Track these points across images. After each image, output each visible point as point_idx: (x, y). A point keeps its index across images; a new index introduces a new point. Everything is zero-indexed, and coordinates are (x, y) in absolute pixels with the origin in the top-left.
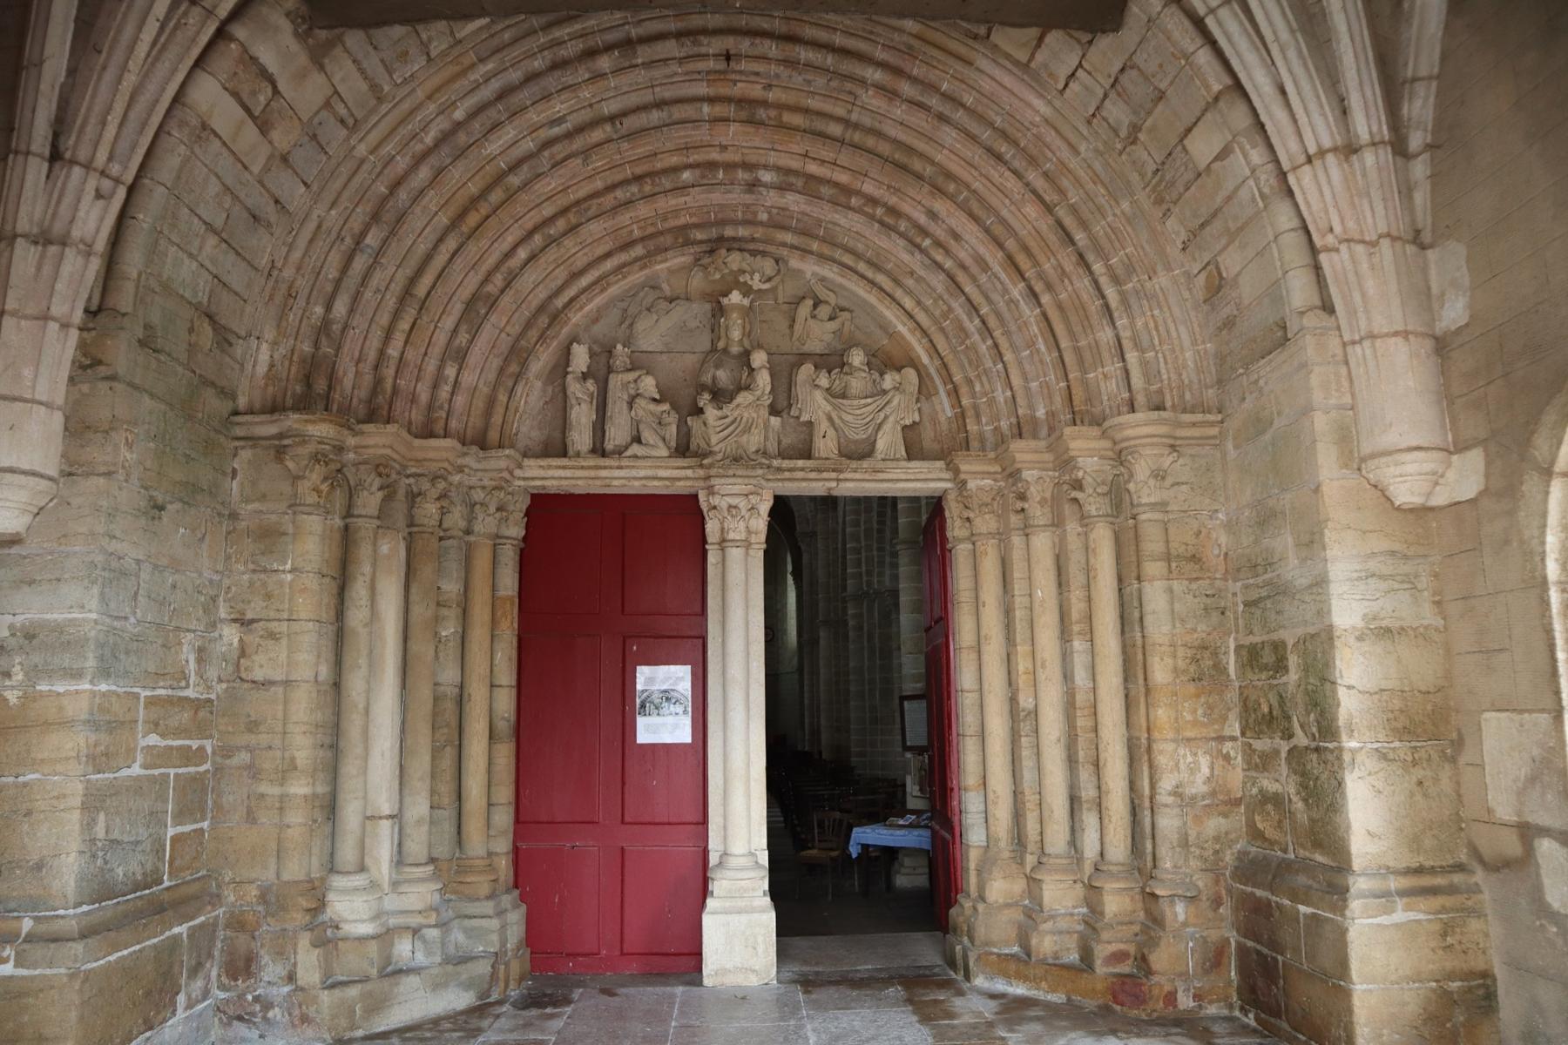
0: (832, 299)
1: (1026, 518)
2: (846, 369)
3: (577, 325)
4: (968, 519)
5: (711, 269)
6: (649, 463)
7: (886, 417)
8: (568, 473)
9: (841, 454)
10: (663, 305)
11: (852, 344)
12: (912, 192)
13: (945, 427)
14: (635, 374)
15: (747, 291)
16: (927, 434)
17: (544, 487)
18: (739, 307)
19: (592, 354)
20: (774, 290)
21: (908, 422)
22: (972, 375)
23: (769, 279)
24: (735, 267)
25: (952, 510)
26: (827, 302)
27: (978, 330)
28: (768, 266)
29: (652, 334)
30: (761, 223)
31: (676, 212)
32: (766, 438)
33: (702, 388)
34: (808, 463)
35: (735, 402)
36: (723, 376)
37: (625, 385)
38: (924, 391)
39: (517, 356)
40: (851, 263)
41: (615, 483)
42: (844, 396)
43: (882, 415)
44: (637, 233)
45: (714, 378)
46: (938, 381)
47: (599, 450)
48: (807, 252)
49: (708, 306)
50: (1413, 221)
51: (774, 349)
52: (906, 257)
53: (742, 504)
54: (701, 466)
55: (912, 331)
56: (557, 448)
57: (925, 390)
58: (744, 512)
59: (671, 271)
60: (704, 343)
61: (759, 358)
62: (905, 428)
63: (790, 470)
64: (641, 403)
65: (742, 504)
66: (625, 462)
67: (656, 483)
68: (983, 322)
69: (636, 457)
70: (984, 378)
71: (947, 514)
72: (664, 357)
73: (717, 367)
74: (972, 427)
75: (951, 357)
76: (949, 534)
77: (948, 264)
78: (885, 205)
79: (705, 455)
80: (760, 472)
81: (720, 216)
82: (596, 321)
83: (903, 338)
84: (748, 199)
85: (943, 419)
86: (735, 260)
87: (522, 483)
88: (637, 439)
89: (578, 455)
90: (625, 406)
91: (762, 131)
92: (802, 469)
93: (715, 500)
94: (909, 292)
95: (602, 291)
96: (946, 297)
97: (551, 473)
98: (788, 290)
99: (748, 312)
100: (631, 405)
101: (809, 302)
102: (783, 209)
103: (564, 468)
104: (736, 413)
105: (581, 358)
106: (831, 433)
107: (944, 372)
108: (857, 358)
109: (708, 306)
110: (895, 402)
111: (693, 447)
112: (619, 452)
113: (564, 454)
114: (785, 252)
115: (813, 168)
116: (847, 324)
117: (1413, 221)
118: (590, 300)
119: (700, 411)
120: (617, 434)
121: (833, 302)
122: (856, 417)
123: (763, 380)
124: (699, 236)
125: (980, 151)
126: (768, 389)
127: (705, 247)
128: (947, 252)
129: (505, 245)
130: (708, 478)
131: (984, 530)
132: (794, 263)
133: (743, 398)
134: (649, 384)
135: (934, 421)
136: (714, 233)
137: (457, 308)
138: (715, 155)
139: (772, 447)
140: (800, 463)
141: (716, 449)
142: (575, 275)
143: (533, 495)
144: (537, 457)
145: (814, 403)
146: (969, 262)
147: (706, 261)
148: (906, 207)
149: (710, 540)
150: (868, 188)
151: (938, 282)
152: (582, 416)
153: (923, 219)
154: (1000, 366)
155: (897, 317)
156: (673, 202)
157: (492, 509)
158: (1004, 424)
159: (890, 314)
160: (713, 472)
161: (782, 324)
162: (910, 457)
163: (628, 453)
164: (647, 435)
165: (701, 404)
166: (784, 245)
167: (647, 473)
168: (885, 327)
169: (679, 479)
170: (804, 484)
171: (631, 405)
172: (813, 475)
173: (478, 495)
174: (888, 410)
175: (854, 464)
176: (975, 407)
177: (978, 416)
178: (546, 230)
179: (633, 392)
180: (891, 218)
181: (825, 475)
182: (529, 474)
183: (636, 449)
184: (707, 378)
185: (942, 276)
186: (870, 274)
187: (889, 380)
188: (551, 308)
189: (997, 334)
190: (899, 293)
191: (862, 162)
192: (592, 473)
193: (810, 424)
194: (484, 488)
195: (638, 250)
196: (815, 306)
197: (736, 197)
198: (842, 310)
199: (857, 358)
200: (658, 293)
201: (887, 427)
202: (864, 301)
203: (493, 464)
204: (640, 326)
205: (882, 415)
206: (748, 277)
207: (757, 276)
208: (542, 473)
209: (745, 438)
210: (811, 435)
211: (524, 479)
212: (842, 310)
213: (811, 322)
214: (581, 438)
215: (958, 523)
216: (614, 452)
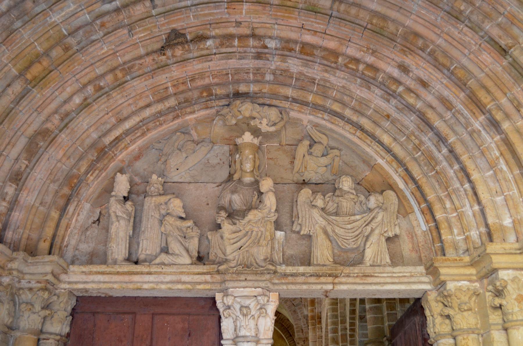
0: (324, 140)
1: (504, 314)
2: (338, 193)
3: (123, 161)
4: (448, 317)
5: (228, 117)
6: (173, 269)
7: (372, 230)
8: (106, 278)
9: (335, 262)
10: (191, 146)
11: (340, 174)
12: (386, 53)
13: (421, 239)
14: (168, 197)
15: (256, 132)
16: (406, 247)
17: (87, 291)
18: (252, 145)
19: (131, 183)
20: (278, 133)
21: (391, 234)
22: (443, 195)
23: (274, 124)
24: (247, 114)
25: (433, 308)
26: (320, 143)
27: (446, 158)
28: (273, 113)
29: (182, 167)
30: (268, 82)
31: (202, 75)
32: (273, 248)
33: (221, 208)
34: (309, 269)
35: (247, 219)
36: (237, 200)
37: (158, 206)
38: (403, 211)
39: (73, 185)
40: (338, 110)
41: (146, 286)
42: (337, 214)
43: (369, 229)
44: (171, 90)
45: (230, 202)
46: (413, 202)
47: (133, 260)
48: (305, 104)
49: (226, 148)
50: (469, 265)
51: (279, 180)
52: (383, 104)
53: (252, 304)
54: (218, 272)
55: (388, 162)
56: (97, 258)
57: (403, 211)
58: (253, 312)
59: (199, 121)
60: (224, 175)
61: (266, 185)
62: (388, 239)
63: (292, 275)
64: (170, 220)
65: (252, 304)
66: (153, 269)
67: (180, 286)
68: (451, 151)
69: (163, 264)
70: (454, 197)
71: (427, 313)
72: (192, 186)
73: (233, 192)
74: (446, 236)
75: (424, 180)
76: (430, 330)
77: (419, 105)
78: (365, 63)
79: (220, 263)
80: (268, 277)
81: (236, 77)
82: (137, 158)
83: (382, 168)
84: (259, 63)
85: (419, 233)
86: (246, 109)
87: (67, 286)
88: (165, 250)
89: (115, 262)
90: (156, 223)
91: (268, 8)
92: (303, 275)
93: (229, 301)
94: (387, 132)
95: (143, 134)
96: (417, 133)
97: (91, 278)
98: (289, 135)
99: (258, 149)
100: (161, 222)
101: (307, 143)
102: (285, 71)
103: (103, 273)
104: (247, 229)
105: (122, 184)
106: (327, 243)
107: (418, 194)
108: (346, 184)
109: (226, 148)
110: (380, 218)
111: (212, 257)
112: (149, 261)
113: (104, 262)
114: (286, 104)
115: (308, 38)
116: (337, 159)
117: (469, 265)
118: (133, 141)
119: (219, 227)
120: (147, 246)
121: (325, 142)
122: (346, 231)
123: (270, 201)
124: (219, 91)
125: (442, 14)
126: (274, 208)
127: (224, 102)
128: (418, 96)
129: (65, 95)
130: (224, 281)
131: (464, 325)
132: (293, 114)
133: (252, 216)
134: (176, 206)
135: (412, 235)
136: (231, 89)
137: (22, 142)
138: (232, 30)
139: (278, 257)
140: (302, 269)
141: (230, 257)
142: (121, 121)
143: (78, 299)
144: (82, 264)
145: (312, 219)
146: (435, 103)
147: (226, 110)
148: (381, 65)
149: (225, 336)
150: (351, 51)
151: (410, 121)
152: (120, 230)
153: (396, 73)
154: (467, 186)
155: (377, 153)
156: (200, 66)
157: (38, 308)
158: (474, 234)
159: (370, 150)
160: (228, 277)
161: (285, 161)
162: (394, 263)
163: (158, 261)
164: (175, 246)
165: (219, 221)
166: (286, 98)
167: (172, 278)
168: (368, 162)
169: (200, 283)
170: (305, 287)
171: (161, 222)
172: (313, 280)
173: (26, 296)
174: (373, 225)
175: (347, 270)
176: (448, 220)
177: (450, 227)
178: (97, 83)
179: (163, 212)
180: (370, 76)
181: (323, 279)
182: (74, 278)
183: (163, 258)
184: (225, 201)
185: (413, 117)
186: (355, 118)
187: (373, 201)
188: (100, 145)
189: (464, 158)
190: (378, 132)
191: (346, 30)
192: (127, 278)
193: (309, 237)
194: (31, 289)
195: (172, 102)
196: (311, 146)
197: (250, 63)
198: (332, 148)
199: (346, 184)
200: (187, 137)
201: (373, 239)
202: (350, 141)
203: (40, 269)
204: (173, 162)
205: (369, 229)
206: (257, 121)
207: (265, 121)
208: (84, 278)
209: (255, 250)
210: (310, 247)
211: (69, 283)
212: (332, 148)
213: (307, 157)
214: (118, 249)
215: (439, 320)
216: (145, 261)
